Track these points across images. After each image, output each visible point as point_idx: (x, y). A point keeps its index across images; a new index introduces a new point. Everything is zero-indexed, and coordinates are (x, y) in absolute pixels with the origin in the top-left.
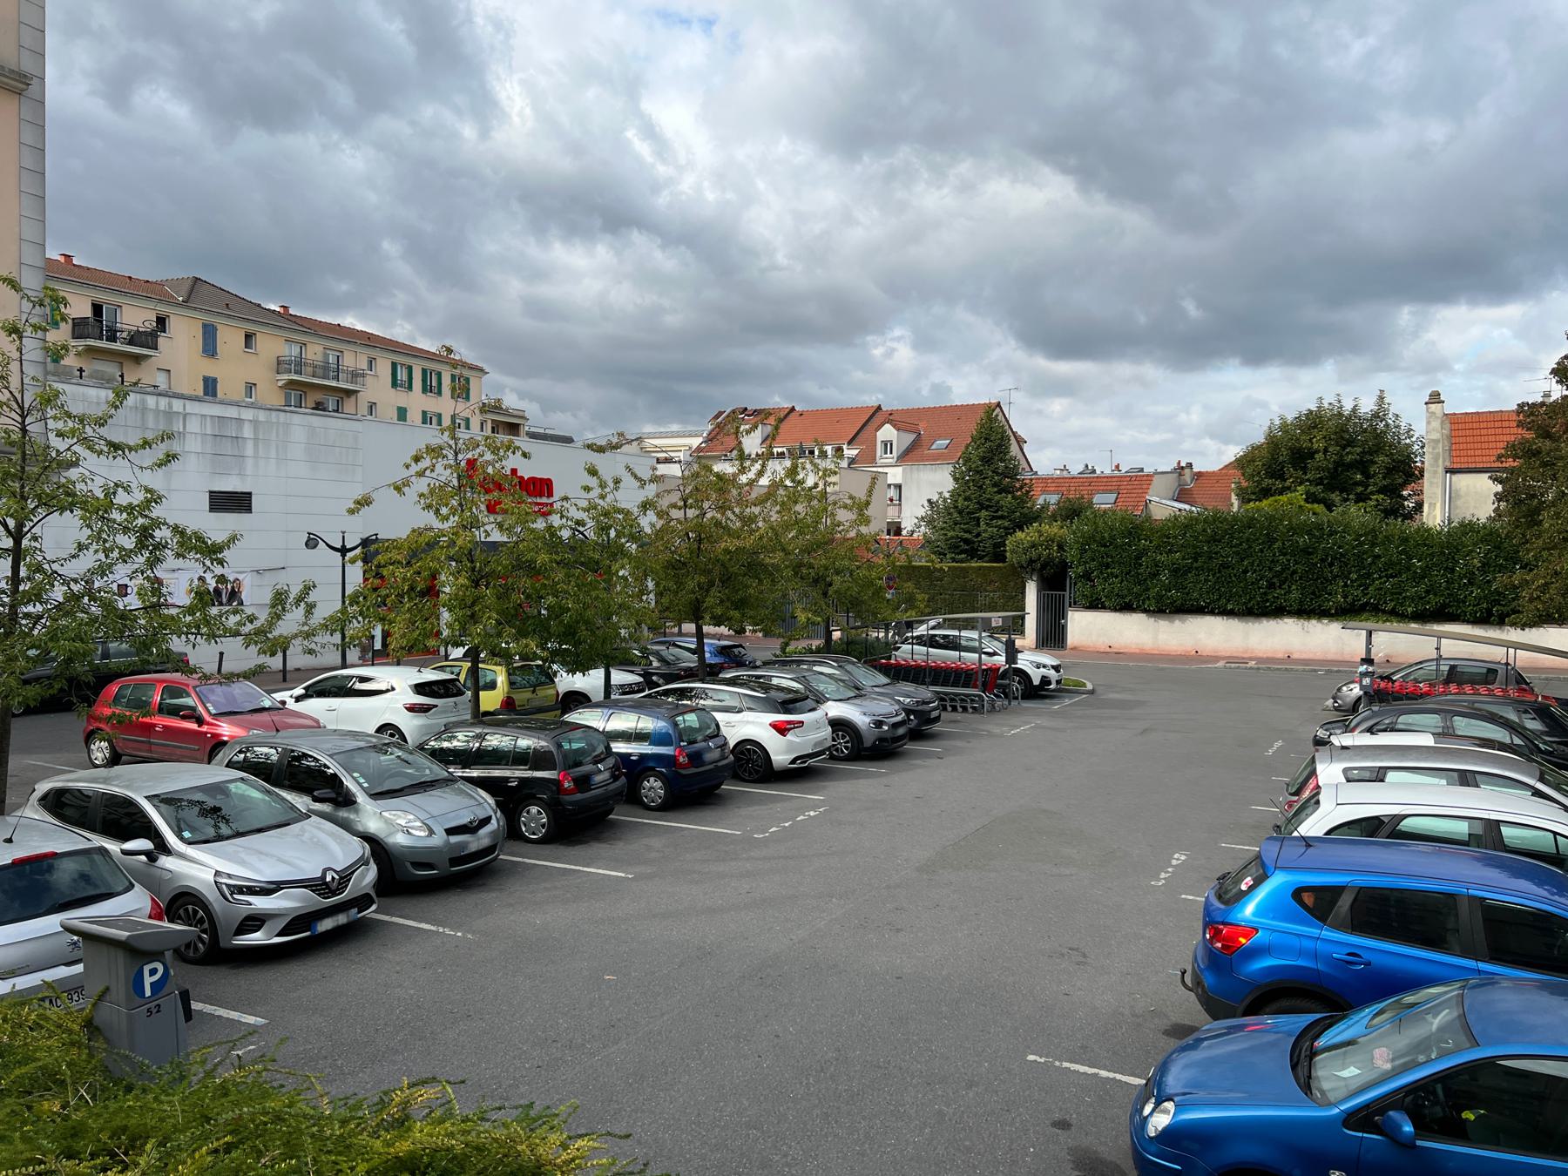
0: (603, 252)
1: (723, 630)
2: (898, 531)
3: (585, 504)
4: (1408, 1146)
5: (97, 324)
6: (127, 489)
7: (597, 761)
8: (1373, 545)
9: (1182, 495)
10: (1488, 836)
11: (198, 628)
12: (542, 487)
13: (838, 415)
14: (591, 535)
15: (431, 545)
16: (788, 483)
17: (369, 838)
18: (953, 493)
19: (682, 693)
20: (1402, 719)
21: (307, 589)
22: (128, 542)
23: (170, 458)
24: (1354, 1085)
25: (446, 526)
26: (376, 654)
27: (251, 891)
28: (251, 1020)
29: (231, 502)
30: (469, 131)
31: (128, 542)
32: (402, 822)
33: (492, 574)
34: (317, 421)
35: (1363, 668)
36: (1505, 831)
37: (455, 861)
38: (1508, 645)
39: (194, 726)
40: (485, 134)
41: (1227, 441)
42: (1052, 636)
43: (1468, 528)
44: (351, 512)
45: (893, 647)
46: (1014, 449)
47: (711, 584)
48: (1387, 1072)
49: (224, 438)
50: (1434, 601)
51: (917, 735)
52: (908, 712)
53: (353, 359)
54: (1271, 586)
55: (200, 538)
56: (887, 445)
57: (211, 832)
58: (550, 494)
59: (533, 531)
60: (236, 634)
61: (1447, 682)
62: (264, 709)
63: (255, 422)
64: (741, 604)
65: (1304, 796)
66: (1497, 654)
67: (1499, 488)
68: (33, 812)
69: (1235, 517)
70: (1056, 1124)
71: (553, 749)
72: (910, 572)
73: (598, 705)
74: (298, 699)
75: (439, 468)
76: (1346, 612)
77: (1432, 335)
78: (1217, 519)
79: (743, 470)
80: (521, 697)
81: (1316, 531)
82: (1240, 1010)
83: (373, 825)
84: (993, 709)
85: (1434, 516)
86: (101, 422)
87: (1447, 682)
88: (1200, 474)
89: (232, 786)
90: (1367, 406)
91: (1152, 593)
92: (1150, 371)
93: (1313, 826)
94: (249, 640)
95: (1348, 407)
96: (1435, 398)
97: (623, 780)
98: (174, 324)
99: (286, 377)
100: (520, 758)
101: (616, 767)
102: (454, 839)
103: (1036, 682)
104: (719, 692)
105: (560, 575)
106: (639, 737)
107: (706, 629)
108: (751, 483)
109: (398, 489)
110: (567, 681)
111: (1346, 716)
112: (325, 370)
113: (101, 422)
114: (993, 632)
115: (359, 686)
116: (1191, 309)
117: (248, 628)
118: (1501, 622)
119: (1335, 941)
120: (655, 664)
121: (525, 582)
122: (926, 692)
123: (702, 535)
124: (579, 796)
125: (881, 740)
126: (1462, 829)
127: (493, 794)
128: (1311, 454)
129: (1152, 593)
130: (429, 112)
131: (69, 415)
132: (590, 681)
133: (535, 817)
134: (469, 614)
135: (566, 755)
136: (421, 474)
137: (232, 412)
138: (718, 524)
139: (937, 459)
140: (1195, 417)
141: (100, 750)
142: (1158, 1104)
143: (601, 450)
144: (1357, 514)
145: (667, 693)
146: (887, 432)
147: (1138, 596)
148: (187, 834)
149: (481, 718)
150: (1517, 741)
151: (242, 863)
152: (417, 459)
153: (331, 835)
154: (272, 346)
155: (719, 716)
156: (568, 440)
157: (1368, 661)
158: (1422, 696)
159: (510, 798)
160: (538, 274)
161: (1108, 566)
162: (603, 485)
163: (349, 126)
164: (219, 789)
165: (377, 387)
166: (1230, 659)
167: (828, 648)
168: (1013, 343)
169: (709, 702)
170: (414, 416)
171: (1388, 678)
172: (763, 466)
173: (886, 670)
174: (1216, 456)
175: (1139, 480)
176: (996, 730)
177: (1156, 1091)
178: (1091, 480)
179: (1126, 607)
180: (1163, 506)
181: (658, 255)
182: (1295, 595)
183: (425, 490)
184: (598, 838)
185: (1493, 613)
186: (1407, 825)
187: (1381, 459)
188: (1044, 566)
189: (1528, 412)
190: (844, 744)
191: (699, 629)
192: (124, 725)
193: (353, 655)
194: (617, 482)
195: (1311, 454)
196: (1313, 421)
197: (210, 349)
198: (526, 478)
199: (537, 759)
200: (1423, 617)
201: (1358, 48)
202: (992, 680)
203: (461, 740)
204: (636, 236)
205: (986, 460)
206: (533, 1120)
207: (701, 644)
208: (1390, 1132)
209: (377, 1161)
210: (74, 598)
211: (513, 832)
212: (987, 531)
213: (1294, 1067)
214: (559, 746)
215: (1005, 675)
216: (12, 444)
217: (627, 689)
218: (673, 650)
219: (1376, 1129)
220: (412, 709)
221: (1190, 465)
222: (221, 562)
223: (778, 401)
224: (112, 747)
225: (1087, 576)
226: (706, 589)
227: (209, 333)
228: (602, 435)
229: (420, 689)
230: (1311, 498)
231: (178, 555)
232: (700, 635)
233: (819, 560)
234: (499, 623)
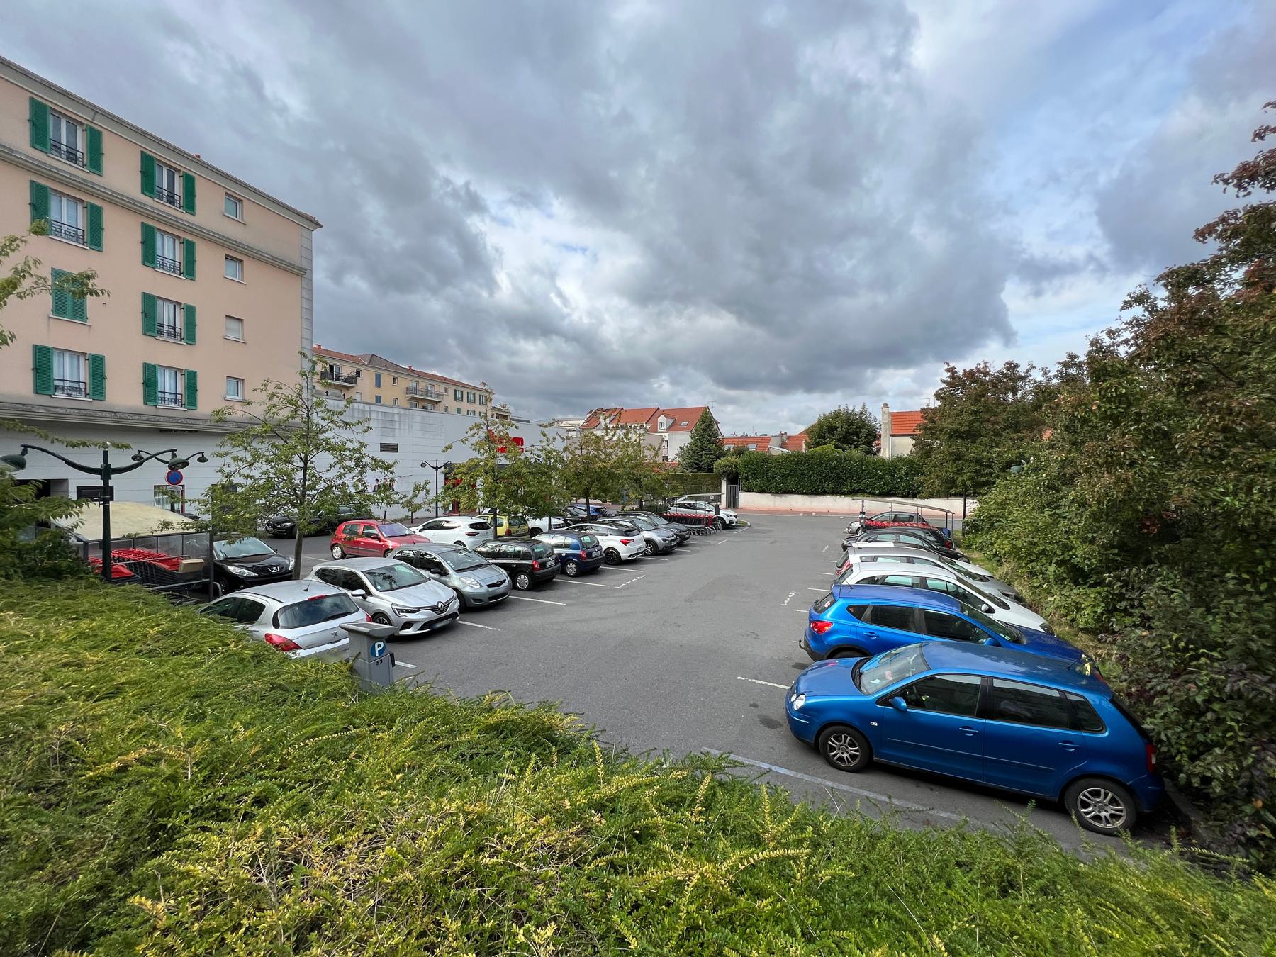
0: (541, 344)
1: (598, 501)
2: (667, 460)
3: (541, 448)
4: (904, 711)
5: (330, 373)
6: (351, 442)
7: (549, 556)
8: (862, 465)
9: (783, 445)
10: (922, 584)
11: (382, 500)
12: (519, 441)
13: (643, 411)
14: (543, 461)
15: (477, 465)
16: (625, 440)
17: (455, 589)
18: (691, 444)
19: (582, 528)
20: (880, 536)
21: (426, 484)
22: (352, 464)
23: (369, 428)
24: (879, 687)
25: (483, 457)
26: (450, 512)
27: (407, 611)
28: (409, 666)
29: (390, 448)
30: (485, 294)
31: (352, 464)
32: (469, 582)
33: (503, 478)
34: (425, 414)
35: (861, 516)
36: (928, 581)
37: (491, 598)
38: (918, 506)
39: (377, 542)
40: (491, 294)
41: (798, 423)
42: (733, 503)
43: (900, 458)
44: (444, 451)
45: (667, 508)
46: (715, 427)
47: (593, 482)
48: (891, 681)
49: (387, 421)
50: (887, 488)
51: (680, 545)
52: (677, 535)
53: (438, 388)
54: (821, 482)
55: (383, 462)
56: (662, 424)
57: (388, 586)
58: (522, 445)
59: (519, 459)
60: (398, 503)
61: (894, 521)
62: (406, 535)
63: (399, 414)
64: (605, 491)
65: (844, 568)
66: (912, 510)
67: (914, 442)
68: (312, 578)
69: (806, 455)
70: (752, 705)
71: (530, 551)
72: (674, 477)
73: (546, 533)
74: (420, 531)
75: (480, 433)
76: (853, 493)
77: (879, 381)
78: (799, 454)
79: (607, 434)
80: (513, 529)
81: (839, 460)
82: (826, 656)
83: (457, 584)
84: (710, 534)
85: (885, 454)
86: (341, 413)
87: (894, 521)
88: (789, 437)
89: (396, 568)
90: (858, 410)
91: (773, 485)
92: (767, 395)
93: (851, 580)
94: (404, 505)
95: (851, 409)
96: (885, 406)
97: (559, 564)
98: (362, 374)
99: (410, 396)
100: (517, 555)
101: (556, 559)
102: (491, 589)
103: (728, 523)
104: (596, 528)
105: (530, 478)
106: (566, 546)
107: (591, 501)
108: (610, 440)
109: (463, 442)
110: (533, 523)
111: (854, 535)
112: (426, 393)
113: (341, 413)
114: (710, 502)
115: (446, 525)
116: (784, 370)
117: (404, 500)
118: (914, 496)
119: (865, 628)
120: (569, 516)
121: (516, 481)
122: (683, 527)
123: (588, 461)
124: (542, 571)
125: (666, 547)
126: (909, 581)
127: (506, 570)
128: (836, 429)
129: (773, 485)
130: (468, 285)
131: (328, 411)
132: (542, 523)
133: (523, 580)
134: (492, 493)
135: (536, 553)
136: (473, 435)
137: (390, 410)
138: (596, 456)
139: (683, 429)
140: (785, 413)
141: (337, 552)
142: (798, 696)
143: (546, 426)
144: (855, 453)
145: (575, 528)
146: (662, 419)
147: (767, 487)
148: (379, 587)
149: (497, 538)
150: (925, 545)
151: (403, 599)
152: (471, 429)
153: (438, 587)
154: (404, 383)
155: (598, 537)
156: (529, 422)
157: (863, 513)
158: (884, 527)
159: (513, 572)
160: (514, 353)
161: (755, 474)
162: (548, 440)
163: (434, 291)
164: (391, 568)
165: (449, 400)
166: (805, 513)
167: (641, 509)
168: (711, 383)
169: (593, 532)
170: (464, 412)
171: (870, 520)
172: (615, 433)
173: (665, 518)
174: (796, 430)
175: (765, 439)
176: (712, 543)
177: (795, 690)
178: (745, 438)
179: (762, 491)
180: (776, 450)
181: (564, 345)
182: (831, 486)
183: (474, 442)
184: (550, 588)
185: (911, 493)
186: (887, 580)
187: (864, 431)
188: (729, 475)
189: (926, 412)
190: (650, 549)
191: (587, 501)
192: (349, 541)
193: (441, 512)
194: (554, 439)
195: (836, 429)
196: (836, 415)
197: (378, 384)
198: (935, 404)
199: (524, 556)
200: (882, 495)
201: (849, 264)
202: (710, 521)
203: (490, 547)
204: (555, 337)
205: (704, 430)
206: (548, 707)
207: (588, 507)
208: (896, 707)
209: (482, 726)
210: (330, 487)
211: (514, 587)
212: (705, 460)
213: (853, 680)
214: (533, 550)
215: (715, 519)
216: (304, 423)
217: (558, 526)
218: (576, 510)
219: (890, 705)
220: (469, 534)
221: (786, 433)
222: (391, 472)
223: (613, 406)
224: (342, 552)
225: (747, 478)
226: (590, 484)
227: (378, 377)
228: (542, 420)
229: (472, 526)
230: (836, 446)
231: (372, 470)
232: (588, 504)
233: (637, 472)
234: (506, 498)
